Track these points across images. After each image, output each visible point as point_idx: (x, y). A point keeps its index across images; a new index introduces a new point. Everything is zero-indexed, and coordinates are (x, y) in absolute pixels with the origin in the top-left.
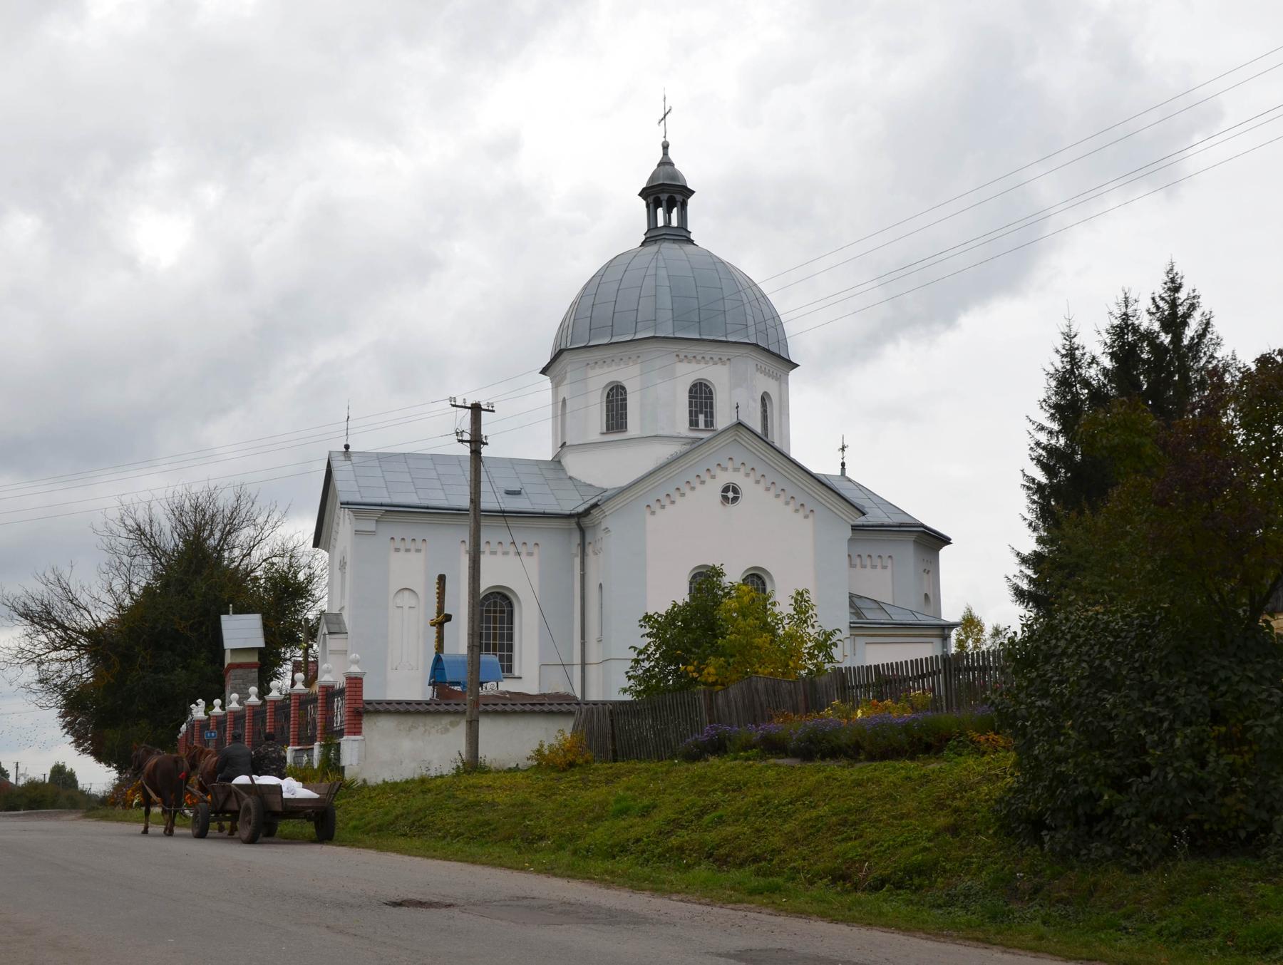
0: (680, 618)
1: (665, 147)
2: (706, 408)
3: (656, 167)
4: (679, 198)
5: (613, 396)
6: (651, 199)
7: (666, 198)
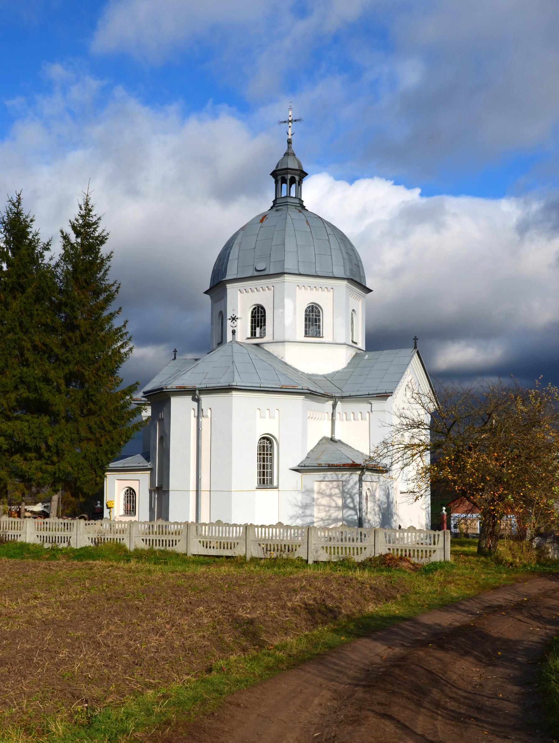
5: (255, 313)
7: (289, 178)
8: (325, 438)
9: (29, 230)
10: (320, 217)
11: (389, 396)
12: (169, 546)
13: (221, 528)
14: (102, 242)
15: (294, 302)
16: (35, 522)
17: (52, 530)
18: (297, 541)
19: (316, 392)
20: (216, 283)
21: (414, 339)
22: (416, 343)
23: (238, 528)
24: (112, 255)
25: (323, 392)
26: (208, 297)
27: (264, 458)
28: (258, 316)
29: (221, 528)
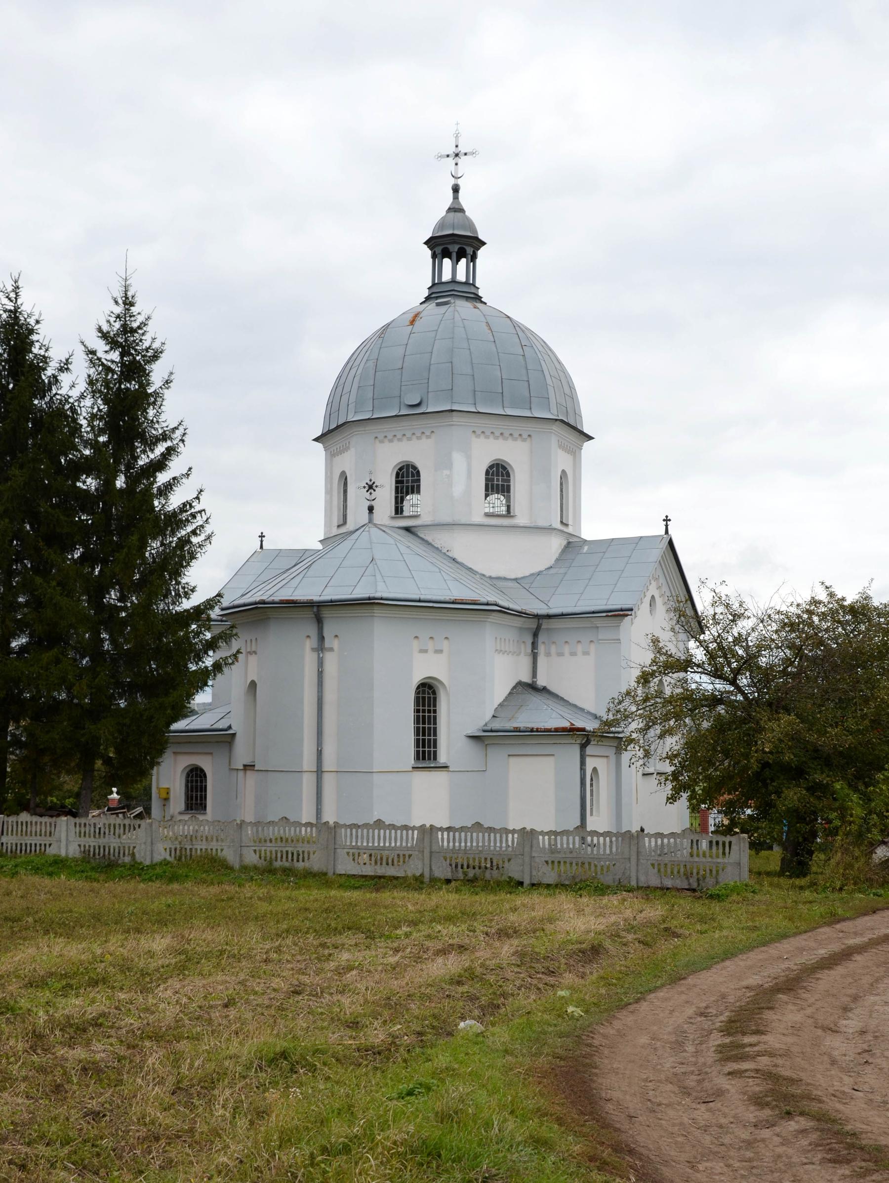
0: (87, 570)
1: (456, 189)
3: (444, 213)
4: (470, 251)
6: (438, 250)
7: (456, 250)
8: (520, 683)
9: (34, 337)
10: (508, 317)
11: (627, 615)
12: (298, 861)
13: (382, 831)
14: (156, 357)
15: (469, 458)
16: (76, 823)
17: (41, 835)
18: (506, 853)
19: (508, 609)
20: (333, 426)
21: (664, 520)
23: (410, 832)
24: (172, 377)
25: (518, 608)
26: (319, 446)
27: (424, 717)
28: (498, 480)
29: (382, 831)
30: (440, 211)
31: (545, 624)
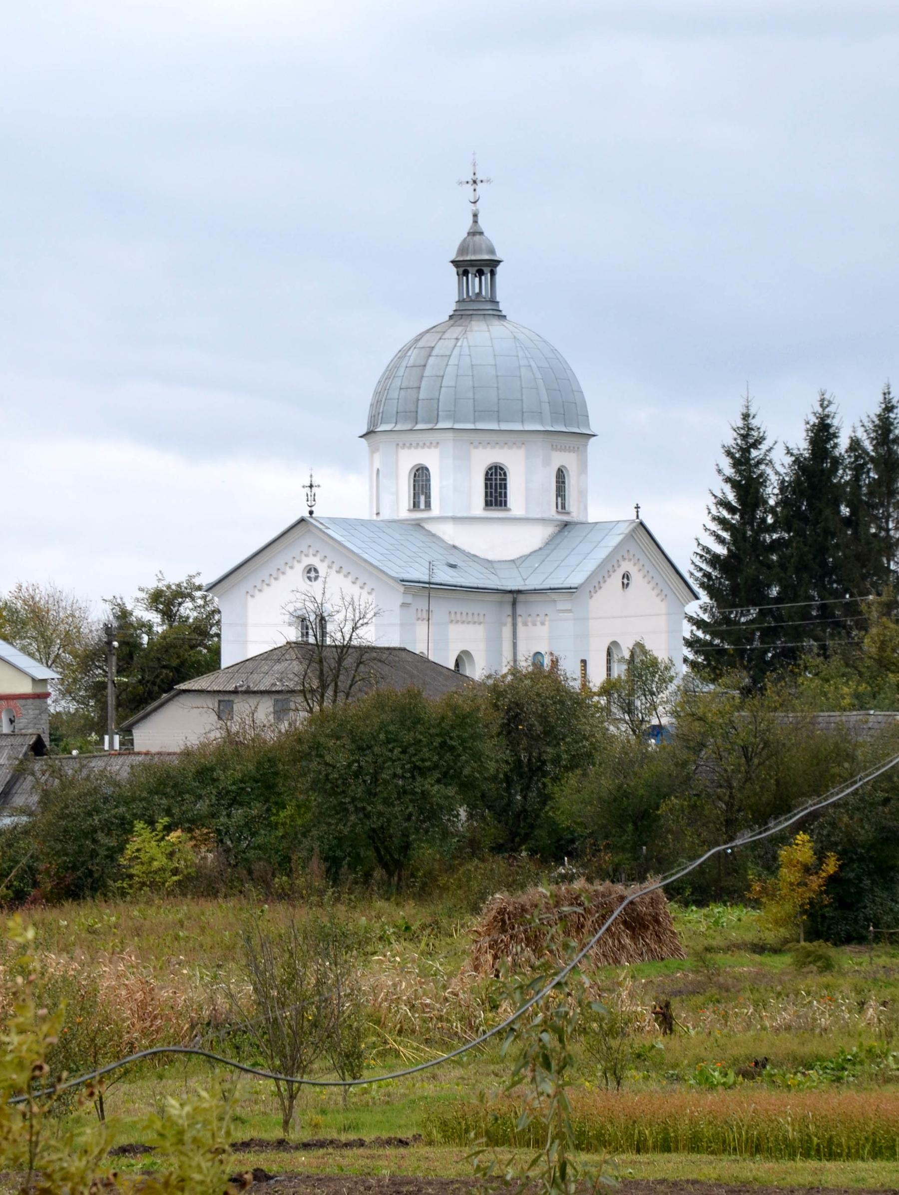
2: (491, 493)
22: (637, 512)
28: (496, 479)
30: (461, 234)
31: (521, 598)
